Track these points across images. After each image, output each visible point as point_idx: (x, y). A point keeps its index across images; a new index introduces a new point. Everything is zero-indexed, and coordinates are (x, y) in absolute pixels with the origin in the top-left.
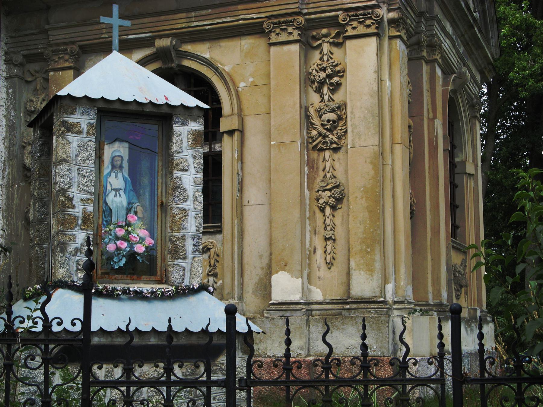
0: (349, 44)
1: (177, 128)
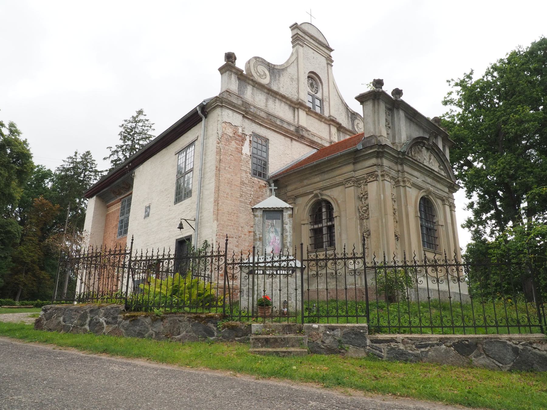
0: (368, 184)
1: (284, 213)
